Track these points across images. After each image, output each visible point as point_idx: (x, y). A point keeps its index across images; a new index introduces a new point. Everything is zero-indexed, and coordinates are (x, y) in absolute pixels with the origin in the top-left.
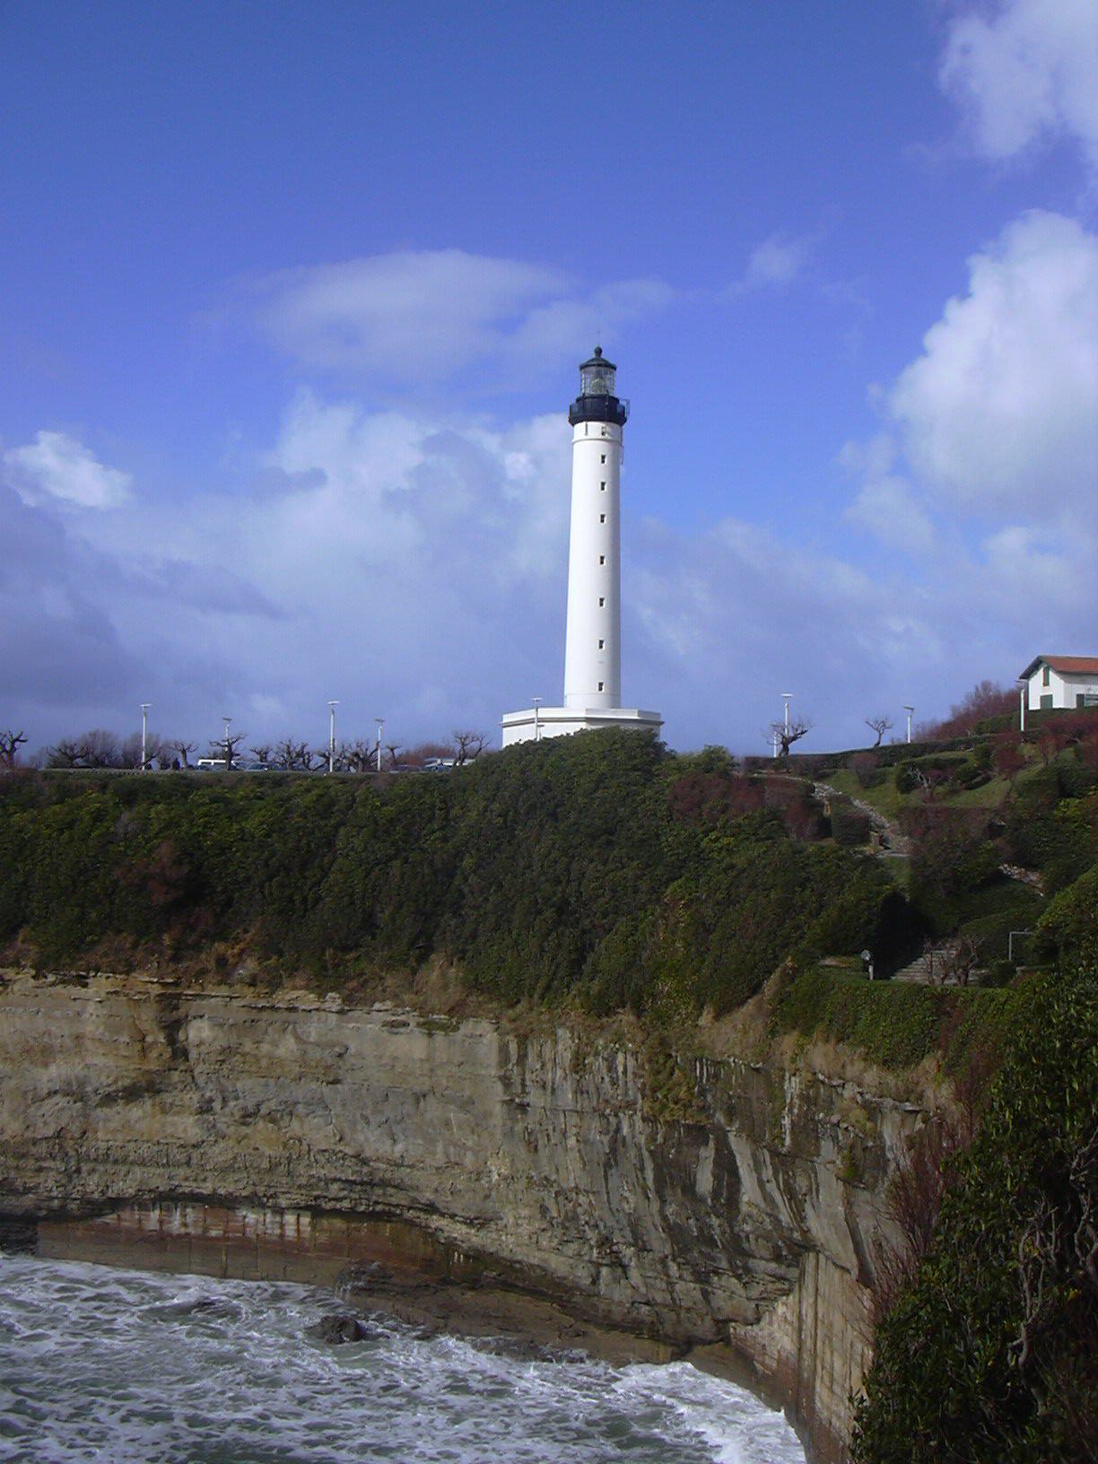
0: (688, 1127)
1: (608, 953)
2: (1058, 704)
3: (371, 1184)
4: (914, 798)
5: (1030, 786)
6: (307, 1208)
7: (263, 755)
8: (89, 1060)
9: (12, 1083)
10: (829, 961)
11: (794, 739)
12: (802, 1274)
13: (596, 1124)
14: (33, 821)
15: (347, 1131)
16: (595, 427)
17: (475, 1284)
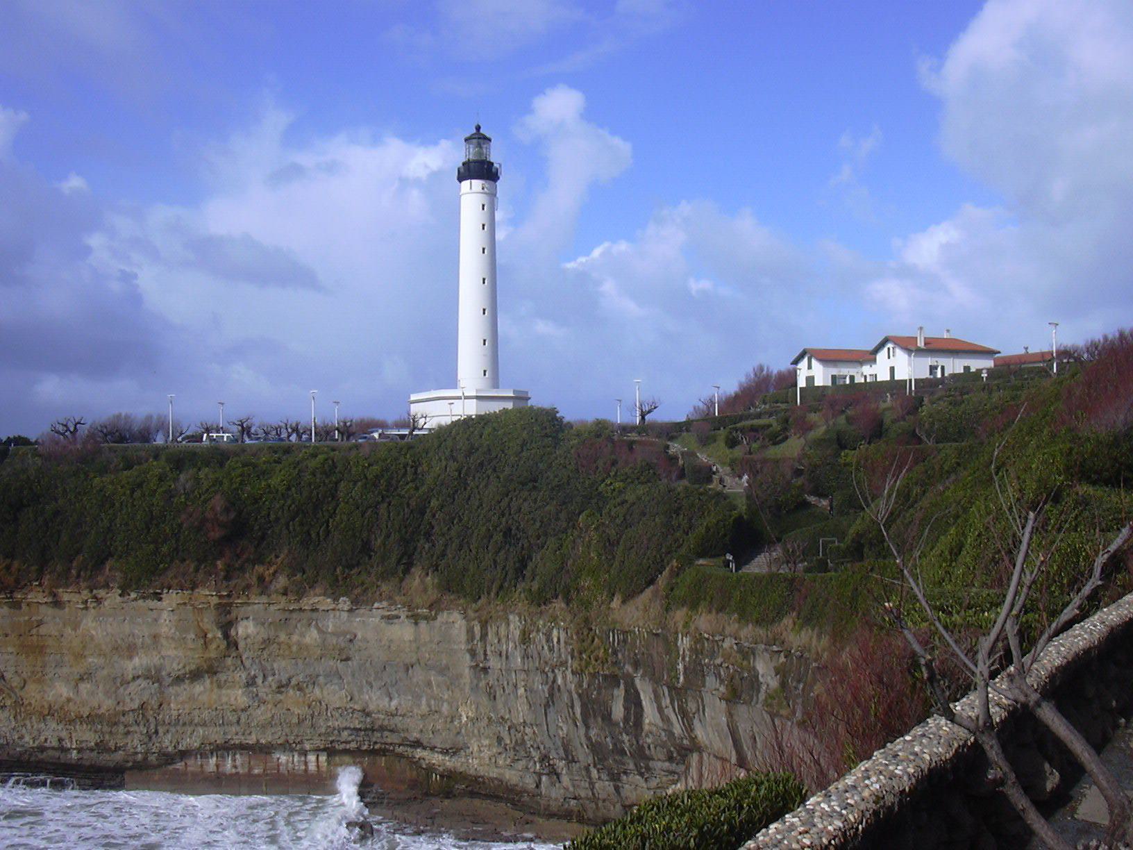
0: (605, 677)
1: (543, 562)
2: (819, 382)
3: (373, 730)
4: (738, 452)
5: (819, 443)
6: (325, 750)
7: (245, 430)
8: (163, 653)
9: (105, 672)
10: (701, 562)
11: (649, 412)
12: (688, 768)
13: (538, 678)
14: (112, 483)
15: (356, 694)
16: (477, 184)
17: (449, 794)
